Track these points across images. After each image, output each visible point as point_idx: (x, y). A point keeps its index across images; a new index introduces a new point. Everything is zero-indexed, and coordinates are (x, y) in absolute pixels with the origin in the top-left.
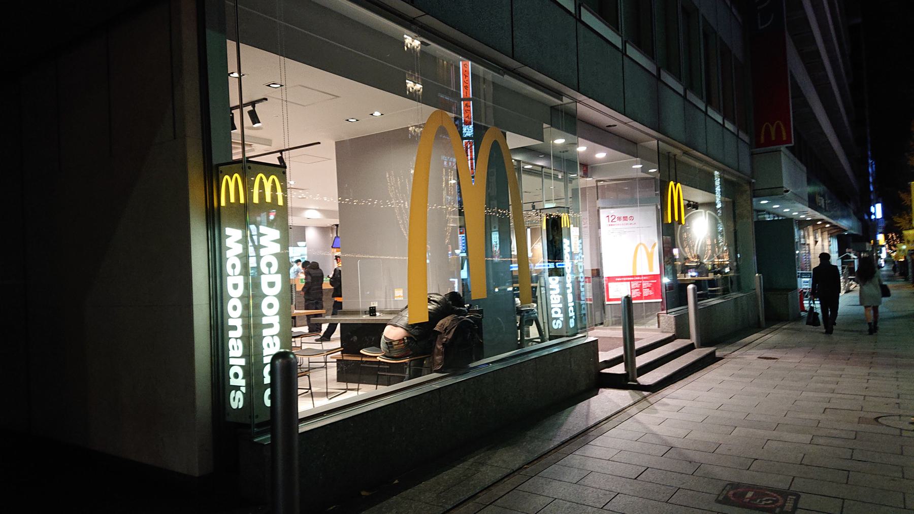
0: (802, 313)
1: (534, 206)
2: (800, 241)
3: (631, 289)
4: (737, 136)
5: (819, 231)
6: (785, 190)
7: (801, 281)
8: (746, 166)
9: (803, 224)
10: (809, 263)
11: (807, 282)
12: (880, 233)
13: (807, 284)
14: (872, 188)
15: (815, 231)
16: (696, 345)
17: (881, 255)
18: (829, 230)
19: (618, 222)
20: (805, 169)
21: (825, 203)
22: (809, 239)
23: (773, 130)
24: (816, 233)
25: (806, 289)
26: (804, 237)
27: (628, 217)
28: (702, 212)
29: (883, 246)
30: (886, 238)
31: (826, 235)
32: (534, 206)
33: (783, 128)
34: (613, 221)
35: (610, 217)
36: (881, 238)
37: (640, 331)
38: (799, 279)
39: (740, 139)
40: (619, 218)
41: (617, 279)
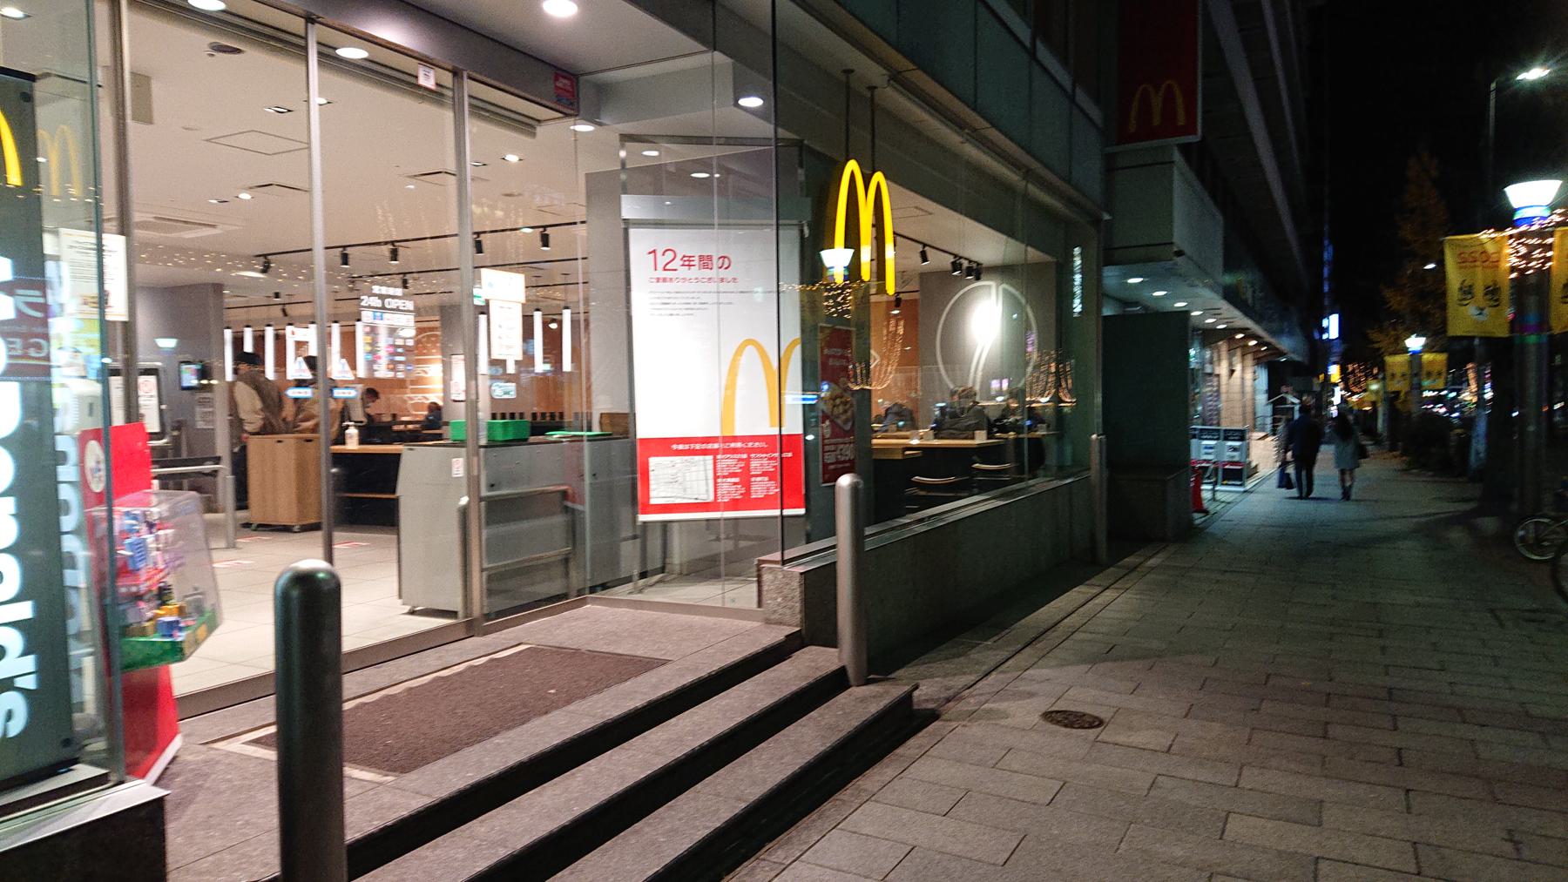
0: (1196, 515)
1: (547, 235)
2: (1203, 369)
3: (716, 477)
4: (1072, 99)
5: (1239, 352)
6: (1175, 249)
7: (1199, 445)
8: (1090, 171)
9: (1209, 337)
10: (1216, 415)
11: (1211, 448)
12: (1334, 363)
13: (1211, 451)
14: (1326, 289)
15: (1231, 351)
16: (851, 673)
17: (1333, 399)
18: (1255, 351)
19: (684, 272)
20: (1219, 217)
21: (1253, 297)
22: (1219, 365)
23: (1157, 102)
24: (1234, 355)
25: (1208, 461)
26: (1211, 362)
27: (715, 260)
28: (990, 286)
29: (1336, 385)
30: (1343, 371)
31: (1249, 359)
32: (547, 235)
33: (1180, 100)
34: (668, 267)
35: (659, 253)
36: (1334, 371)
37: (707, 614)
38: (1194, 441)
39: (1078, 106)
40: (687, 262)
41: (675, 447)
